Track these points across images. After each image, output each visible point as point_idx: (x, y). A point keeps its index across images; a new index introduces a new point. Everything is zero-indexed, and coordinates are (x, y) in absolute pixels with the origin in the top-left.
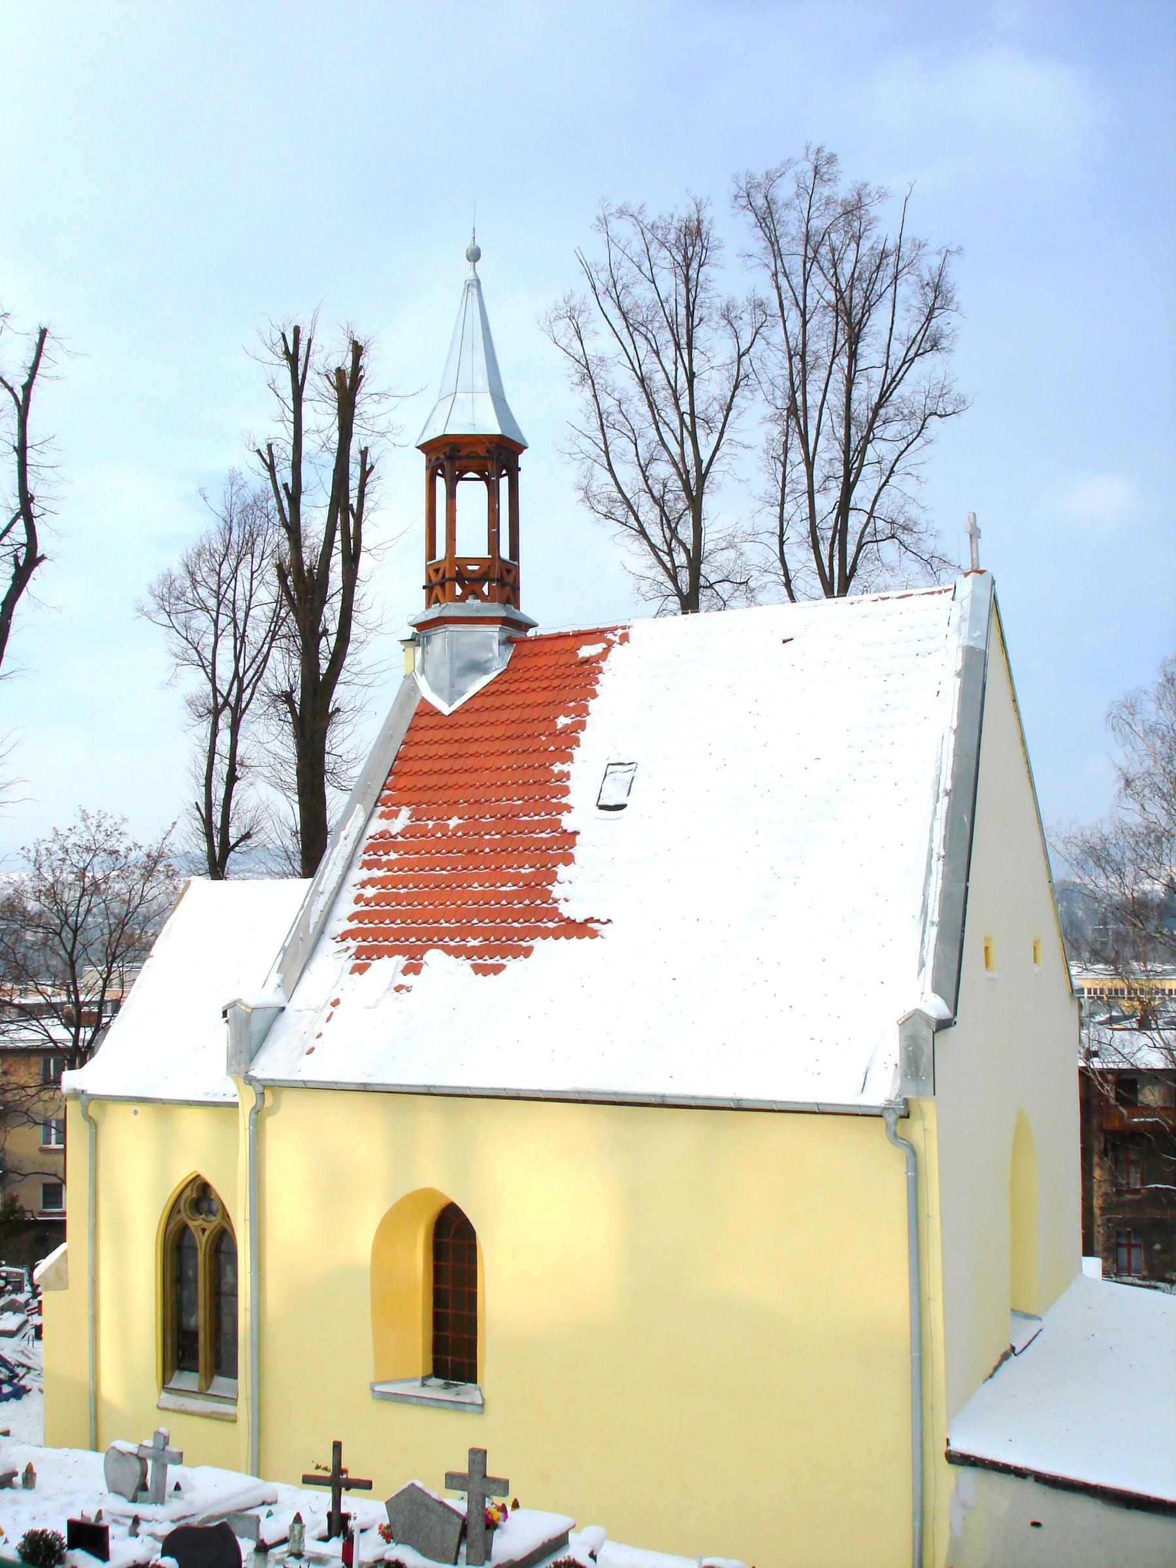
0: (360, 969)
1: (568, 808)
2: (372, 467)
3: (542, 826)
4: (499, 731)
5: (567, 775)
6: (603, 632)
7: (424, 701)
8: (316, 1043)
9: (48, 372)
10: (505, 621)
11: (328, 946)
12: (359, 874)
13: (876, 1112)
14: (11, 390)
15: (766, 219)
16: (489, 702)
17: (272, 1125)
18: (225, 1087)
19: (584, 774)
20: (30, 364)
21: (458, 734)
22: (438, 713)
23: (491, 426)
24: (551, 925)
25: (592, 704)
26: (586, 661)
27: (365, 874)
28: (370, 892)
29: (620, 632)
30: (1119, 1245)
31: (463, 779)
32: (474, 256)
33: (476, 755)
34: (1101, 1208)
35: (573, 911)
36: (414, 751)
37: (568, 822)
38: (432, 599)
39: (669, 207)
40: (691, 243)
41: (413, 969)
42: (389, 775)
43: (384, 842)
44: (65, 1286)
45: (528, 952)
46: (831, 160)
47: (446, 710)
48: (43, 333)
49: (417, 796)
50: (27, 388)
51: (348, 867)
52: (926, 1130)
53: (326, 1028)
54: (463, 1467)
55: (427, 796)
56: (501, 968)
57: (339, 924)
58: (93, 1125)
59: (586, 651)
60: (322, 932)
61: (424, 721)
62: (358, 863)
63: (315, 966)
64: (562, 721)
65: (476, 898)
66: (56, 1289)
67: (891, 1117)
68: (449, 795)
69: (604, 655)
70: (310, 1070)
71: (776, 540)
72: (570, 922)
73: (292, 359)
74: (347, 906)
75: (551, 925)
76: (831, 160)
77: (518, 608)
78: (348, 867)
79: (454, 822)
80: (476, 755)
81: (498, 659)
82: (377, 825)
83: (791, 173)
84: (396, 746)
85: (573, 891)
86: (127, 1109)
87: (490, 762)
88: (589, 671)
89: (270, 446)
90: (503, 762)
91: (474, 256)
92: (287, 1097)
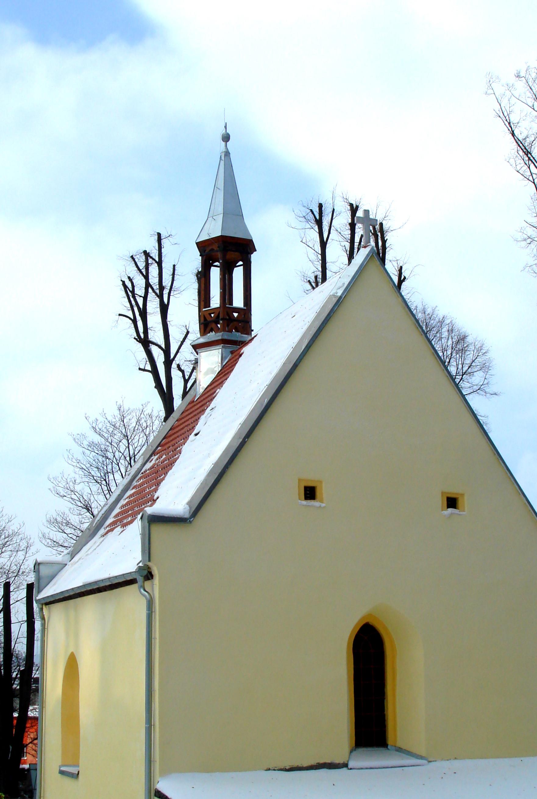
32: (226, 138)
67: (140, 579)
68: (168, 445)
73: (319, 222)
91: (226, 138)
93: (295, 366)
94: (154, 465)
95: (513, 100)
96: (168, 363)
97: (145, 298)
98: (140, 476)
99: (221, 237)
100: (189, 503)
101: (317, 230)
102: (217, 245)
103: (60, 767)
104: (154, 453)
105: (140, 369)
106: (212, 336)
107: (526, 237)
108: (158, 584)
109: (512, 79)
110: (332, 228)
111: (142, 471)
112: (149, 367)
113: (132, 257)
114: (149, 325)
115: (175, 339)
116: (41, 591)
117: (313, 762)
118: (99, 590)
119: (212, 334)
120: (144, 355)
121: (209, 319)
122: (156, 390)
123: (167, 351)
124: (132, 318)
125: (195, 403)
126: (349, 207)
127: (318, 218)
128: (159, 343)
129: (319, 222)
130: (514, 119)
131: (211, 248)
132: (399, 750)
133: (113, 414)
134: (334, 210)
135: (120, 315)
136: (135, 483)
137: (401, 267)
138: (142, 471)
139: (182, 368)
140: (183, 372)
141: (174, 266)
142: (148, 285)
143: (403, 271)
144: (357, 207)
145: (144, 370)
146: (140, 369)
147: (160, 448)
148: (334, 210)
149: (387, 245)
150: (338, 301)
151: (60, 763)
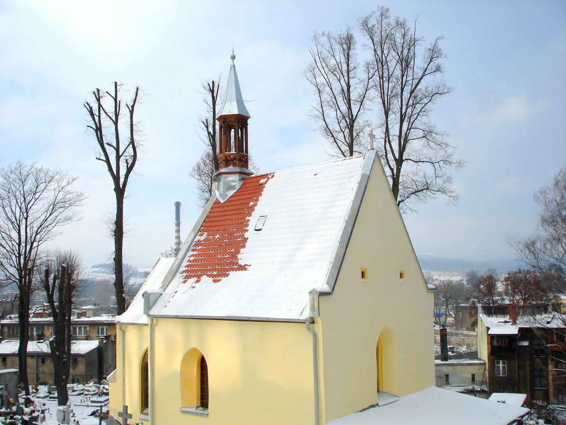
0: (185, 282)
1: (247, 231)
3: (239, 237)
4: (234, 208)
5: (249, 220)
6: (267, 175)
7: (217, 199)
8: (168, 304)
9: (140, 101)
10: (240, 173)
11: (178, 275)
12: (190, 253)
14: (128, 107)
15: (371, 33)
16: (236, 198)
17: (156, 329)
18: (145, 320)
19: (253, 221)
20: (134, 99)
21: (226, 209)
22: (220, 203)
23: (235, 111)
24: (236, 267)
25: (260, 198)
26: (261, 184)
27: (192, 253)
28: (192, 258)
29: (272, 175)
30: (559, 393)
31: (221, 223)
32: (233, 58)
33: (227, 215)
34: (552, 380)
35: (241, 262)
36: (213, 215)
37: (246, 235)
39: (340, 31)
40: (348, 43)
41: (198, 281)
43: (199, 243)
44: (116, 382)
45: (228, 275)
46: (387, 10)
47: (222, 202)
48: (137, 89)
49: (208, 229)
50: (133, 106)
51: (187, 251)
52: (319, 327)
53: (172, 300)
54: (122, 411)
55: (211, 229)
56: (221, 280)
57: (183, 268)
58: (124, 333)
59: (262, 181)
60: (177, 271)
61: (217, 205)
63: (173, 282)
64: (252, 203)
65: (220, 259)
67: (307, 323)
68: (217, 228)
69: (266, 183)
70: (165, 312)
71: (384, 140)
72: (241, 266)
73: (212, 91)
74: (185, 263)
75: (236, 267)
76: (387, 10)
78: (187, 251)
79: (217, 236)
80: (227, 215)
81: (238, 185)
82: (198, 238)
83: (374, 16)
84: (207, 213)
85: (243, 257)
86: (132, 327)
87: (229, 217)
88: (262, 186)
89: (207, 120)
90: (233, 217)
91: (233, 58)
92: (160, 320)
96: (118, 157)
97: (99, 117)
103: (181, 408)
105: (97, 158)
107: (313, 114)
108: (321, 327)
111: (196, 240)
117: (368, 406)
121: (229, 159)
123: (117, 149)
129: (212, 91)
132: (390, 394)
138: (196, 240)
140: (128, 163)
145: (100, 159)
146: (97, 158)
151: (180, 406)
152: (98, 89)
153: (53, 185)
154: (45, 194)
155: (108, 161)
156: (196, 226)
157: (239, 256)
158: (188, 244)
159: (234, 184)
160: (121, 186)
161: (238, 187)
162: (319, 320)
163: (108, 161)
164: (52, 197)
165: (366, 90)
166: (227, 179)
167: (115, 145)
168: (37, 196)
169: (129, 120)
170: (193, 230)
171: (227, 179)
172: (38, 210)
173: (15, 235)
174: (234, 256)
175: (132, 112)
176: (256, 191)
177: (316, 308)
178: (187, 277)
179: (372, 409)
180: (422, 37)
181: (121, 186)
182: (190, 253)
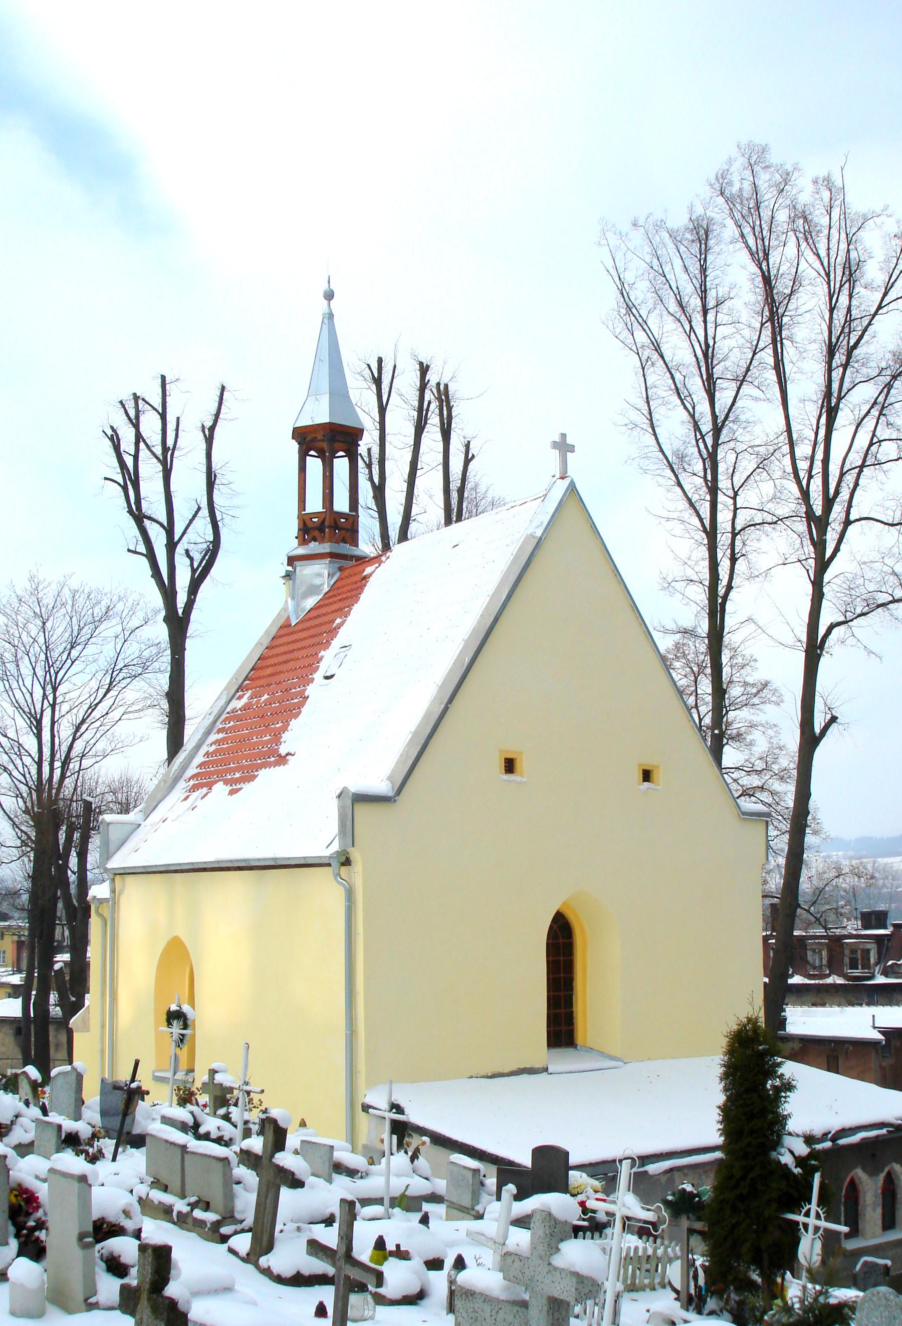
2: (473, 456)
10: (333, 555)
11: (182, 784)
12: (213, 737)
13: (327, 861)
32: (329, 296)
38: (303, 542)
40: (702, 234)
42: (252, 670)
44: (88, 1031)
45: (253, 778)
48: (223, 388)
52: (358, 874)
57: (192, 770)
61: (286, 631)
62: (215, 730)
66: (83, 1032)
67: (335, 863)
73: (378, 381)
75: (272, 759)
77: (357, 546)
91: (329, 296)
93: (496, 620)
94: (246, 704)
95: (630, 255)
96: (171, 546)
97: (136, 458)
98: (224, 716)
99: (330, 424)
100: (390, 778)
101: (375, 391)
102: (322, 432)
103: (154, 1072)
104: (240, 688)
105: (129, 550)
106: (314, 547)
108: (361, 871)
109: (626, 227)
110: (393, 389)
111: (228, 709)
112: (142, 549)
113: (121, 402)
114: (143, 495)
115: (182, 516)
116: (111, 857)
118: (251, 868)
119: (313, 544)
120: (136, 531)
121: (310, 525)
122: (153, 579)
123: (169, 530)
124: (122, 483)
125: (292, 630)
126: (418, 367)
127: (376, 375)
128: (160, 520)
129: (378, 381)
130: (629, 277)
131: (313, 435)
133: (22, 586)
134: (395, 366)
135: (106, 479)
136: (219, 725)
137: (469, 442)
138: (228, 709)
139: (191, 554)
140: (192, 559)
141: (178, 418)
142: (139, 437)
143: (471, 447)
144: (428, 367)
145: (135, 552)
146: (129, 550)
147: (247, 682)
148: (395, 366)
149: (453, 414)
150: (538, 543)
152: (135, 394)
153: (110, 629)
154: (91, 649)
155: (151, 556)
156: (235, 677)
157: (285, 736)
158: (212, 718)
159: (317, 581)
160: (180, 611)
161: (326, 589)
162: (356, 855)
163: (151, 556)
164: (109, 651)
165: (755, 354)
166: (304, 572)
167: (164, 519)
168: (75, 653)
169: (204, 460)
170: (225, 689)
171: (304, 572)
172: (78, 685)
173: (30, 743)
174: (277, 739)
175: (209, 441)
176: (354, 593)
177: (348, 828)
178: (194, 788)
179: (525, 1077)
180: (886, 208)
181: (180, 611)
182: (213, 737)
